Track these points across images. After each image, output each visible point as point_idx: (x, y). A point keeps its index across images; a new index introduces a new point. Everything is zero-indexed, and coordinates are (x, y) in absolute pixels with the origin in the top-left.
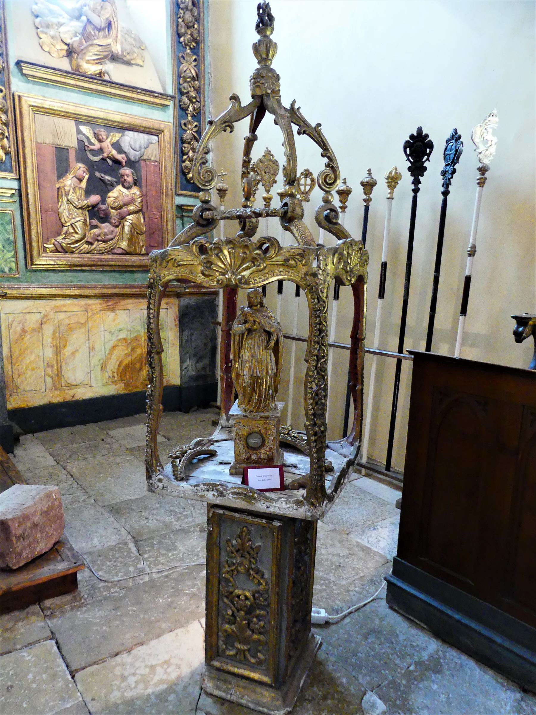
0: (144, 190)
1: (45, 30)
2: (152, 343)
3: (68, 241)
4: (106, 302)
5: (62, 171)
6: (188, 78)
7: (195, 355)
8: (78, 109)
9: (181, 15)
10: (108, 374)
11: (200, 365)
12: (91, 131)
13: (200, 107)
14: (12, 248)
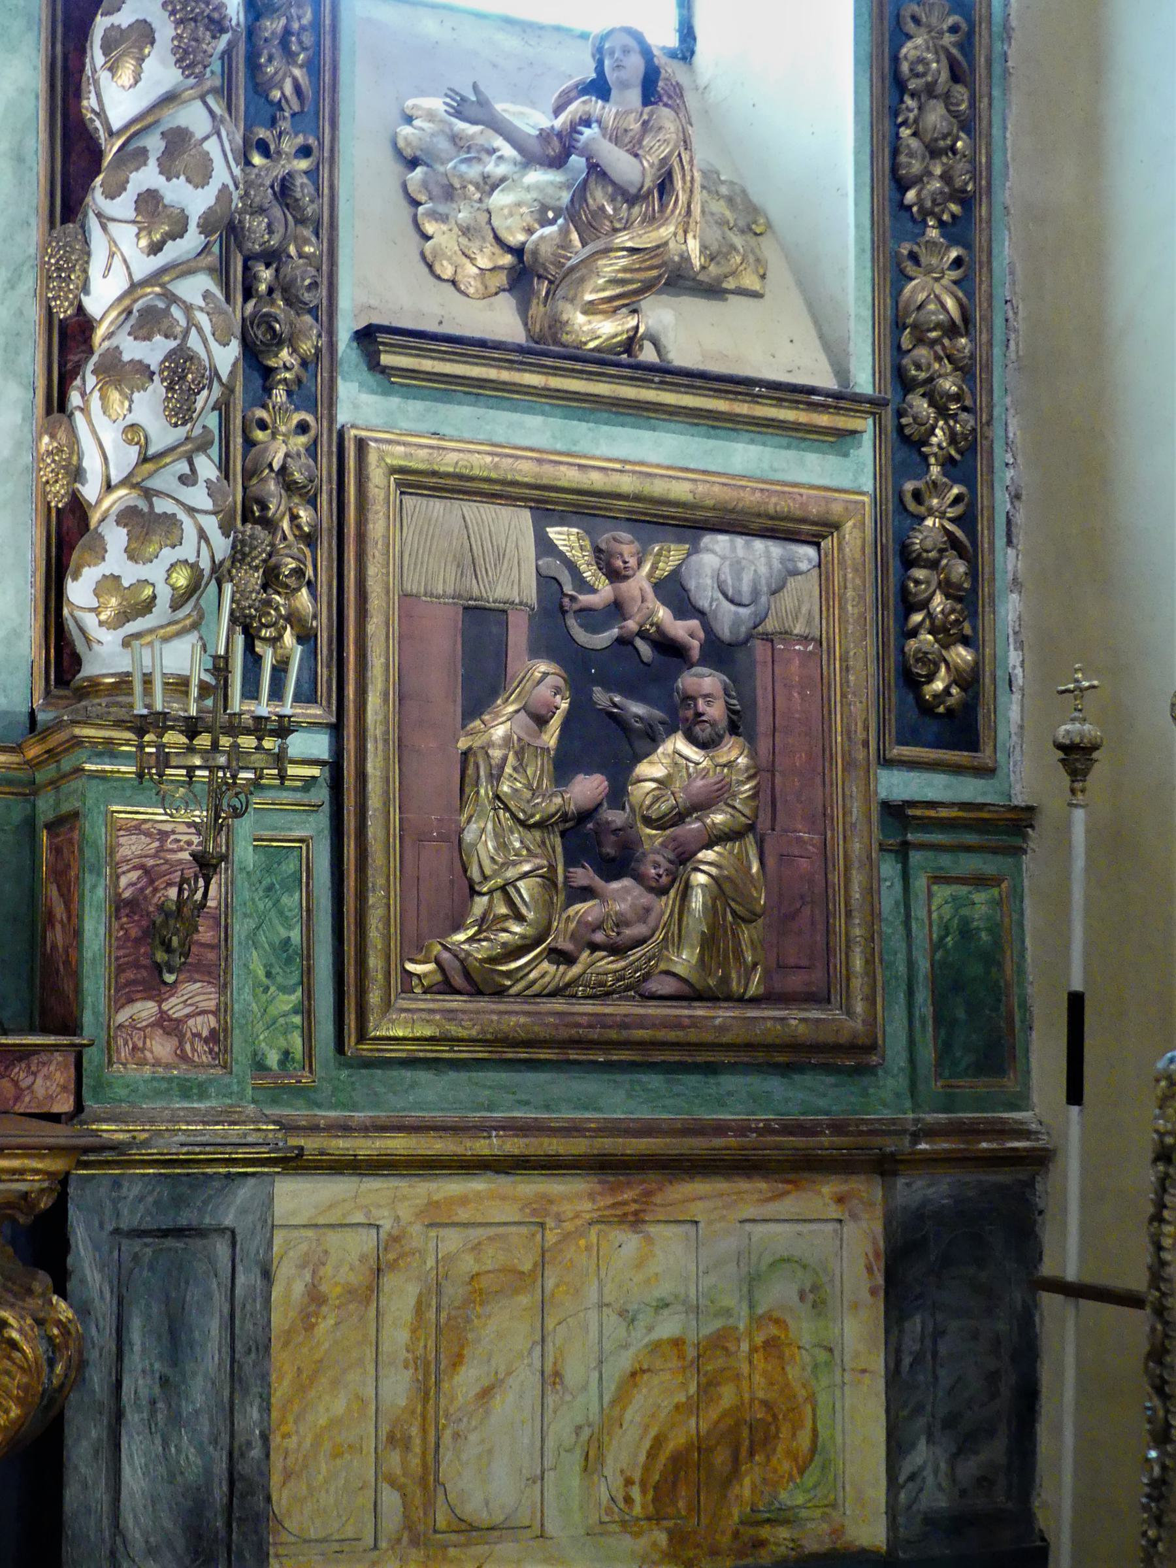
0: (764, 745)
1: (442, 208)
2: (1166, 1323)
3: (480, 951)
4: (613, 1190)
5: (481, 688)
6: (934, 329)
7: (950, 1422)
8: (548, 469)
9: (912, 116)
10: (609, 1485)
11: (970, 1467)
12: (587, 543)
13: (974, 430)
14: (295, 978)
